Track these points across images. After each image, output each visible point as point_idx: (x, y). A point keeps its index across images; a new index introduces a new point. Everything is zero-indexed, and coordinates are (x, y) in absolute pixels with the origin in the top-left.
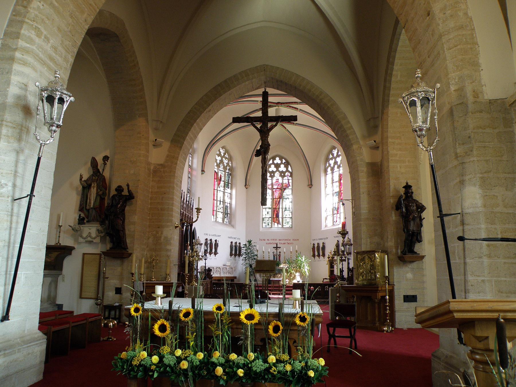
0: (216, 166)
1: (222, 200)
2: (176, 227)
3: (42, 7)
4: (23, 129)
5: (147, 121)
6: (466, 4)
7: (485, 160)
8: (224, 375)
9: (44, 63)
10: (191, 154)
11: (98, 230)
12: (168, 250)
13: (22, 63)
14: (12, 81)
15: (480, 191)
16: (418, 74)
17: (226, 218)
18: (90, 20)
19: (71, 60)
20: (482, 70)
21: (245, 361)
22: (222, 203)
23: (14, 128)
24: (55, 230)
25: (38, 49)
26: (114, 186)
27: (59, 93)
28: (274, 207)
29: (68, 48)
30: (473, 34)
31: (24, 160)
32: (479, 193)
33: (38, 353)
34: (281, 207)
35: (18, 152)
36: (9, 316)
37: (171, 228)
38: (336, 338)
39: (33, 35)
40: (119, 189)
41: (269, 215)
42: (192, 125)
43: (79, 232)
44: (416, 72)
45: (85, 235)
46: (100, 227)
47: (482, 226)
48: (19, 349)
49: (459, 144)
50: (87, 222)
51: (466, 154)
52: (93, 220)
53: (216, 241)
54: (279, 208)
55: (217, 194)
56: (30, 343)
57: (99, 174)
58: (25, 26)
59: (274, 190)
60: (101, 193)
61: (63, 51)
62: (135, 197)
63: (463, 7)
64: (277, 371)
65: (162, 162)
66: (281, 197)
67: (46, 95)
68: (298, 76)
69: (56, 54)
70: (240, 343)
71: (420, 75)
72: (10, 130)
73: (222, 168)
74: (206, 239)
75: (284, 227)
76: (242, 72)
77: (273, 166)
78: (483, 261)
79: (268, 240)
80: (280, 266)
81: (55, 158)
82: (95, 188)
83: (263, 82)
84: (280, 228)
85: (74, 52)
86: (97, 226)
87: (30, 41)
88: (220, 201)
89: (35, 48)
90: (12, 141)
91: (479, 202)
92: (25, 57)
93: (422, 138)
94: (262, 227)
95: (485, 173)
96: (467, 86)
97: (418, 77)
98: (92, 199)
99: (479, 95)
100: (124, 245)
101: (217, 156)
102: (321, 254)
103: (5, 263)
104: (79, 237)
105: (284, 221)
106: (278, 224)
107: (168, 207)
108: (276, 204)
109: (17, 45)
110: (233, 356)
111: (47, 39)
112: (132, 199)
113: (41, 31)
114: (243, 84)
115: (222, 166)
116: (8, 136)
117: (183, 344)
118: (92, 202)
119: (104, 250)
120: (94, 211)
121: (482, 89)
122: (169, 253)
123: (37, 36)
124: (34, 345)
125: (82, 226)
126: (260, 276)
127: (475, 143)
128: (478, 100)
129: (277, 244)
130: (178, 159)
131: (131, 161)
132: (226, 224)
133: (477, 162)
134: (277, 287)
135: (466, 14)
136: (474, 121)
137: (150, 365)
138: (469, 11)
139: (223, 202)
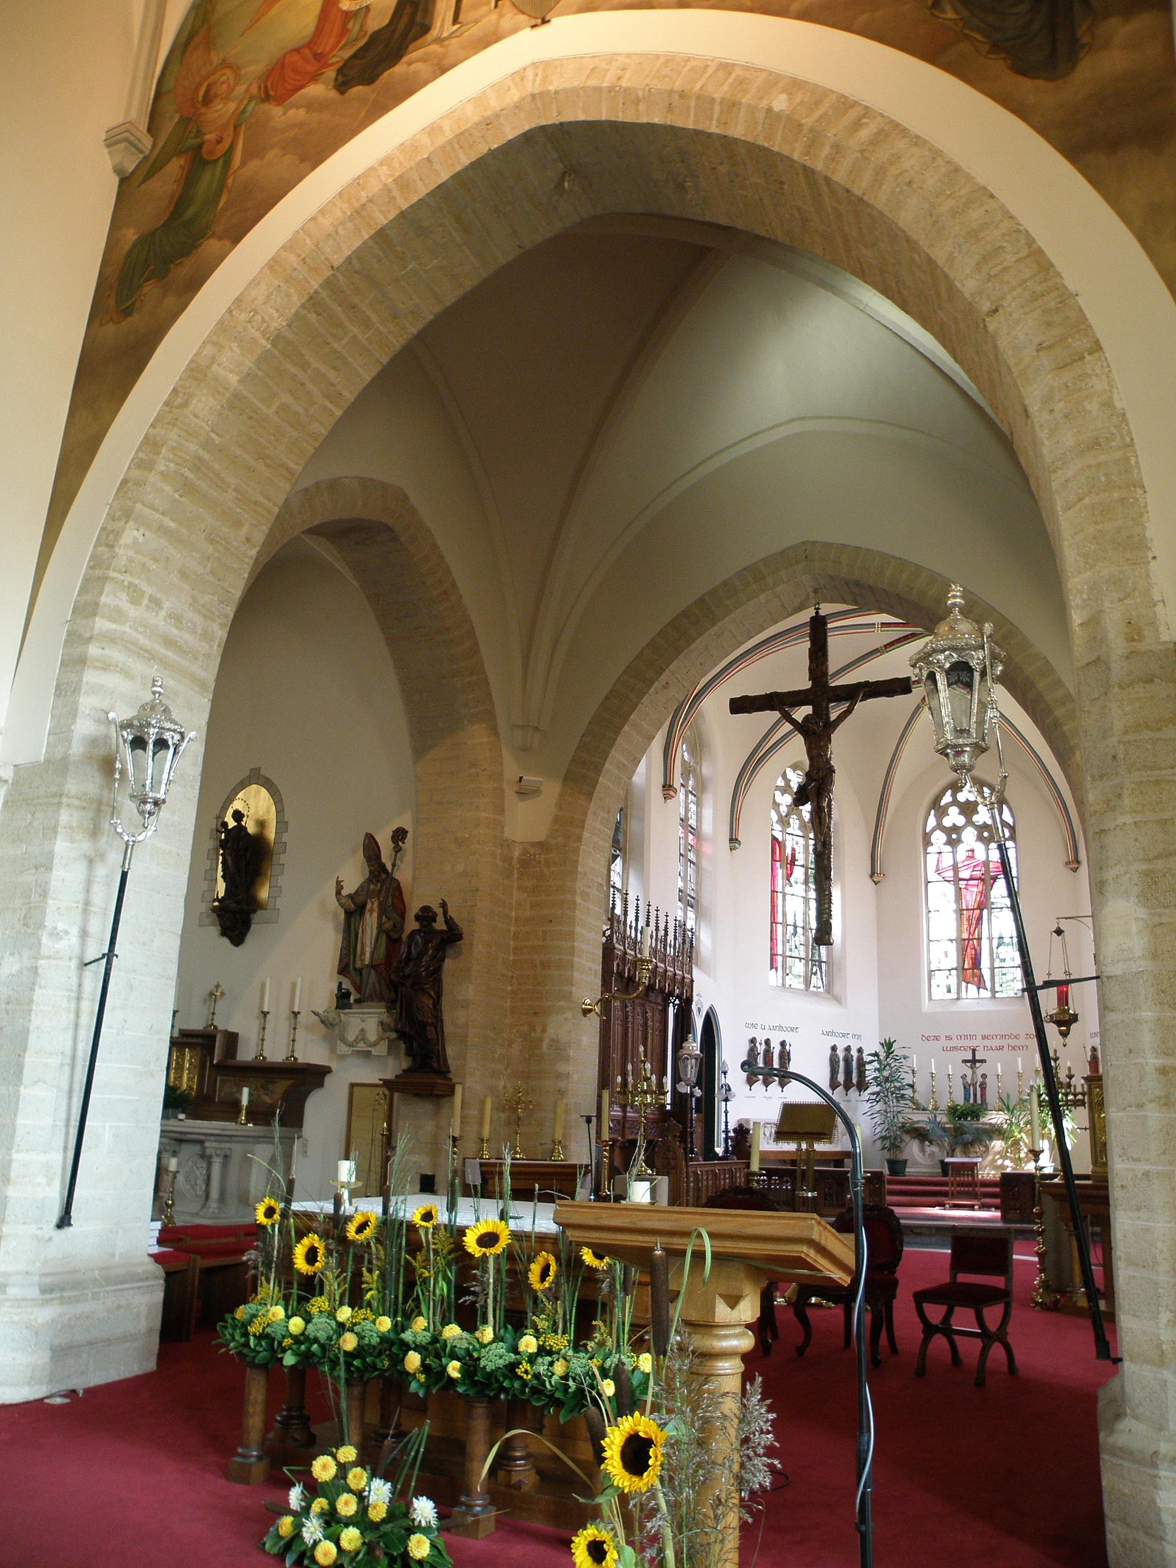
0: (777, 822)
1: (800, 923)
2: (586, 1012)
3: (141, 539)
4: (103, 808)
5: (494, 731)
6: (1108, 377)
7: (1158, 821)
8: (422, 1372)
9: (150, 656)
10: (692, 794)
11: (382, 1023)
12: (559, 1076)
13: (102, 665)
14: (81, 709)
15: (1142, 912)
16: (954, 597)
17: (815, 974)
18: (259, 537)
19: (220, 634)
20: (1154, 558)
21: (470, 1344)
22: (800, 931)
23: (84, 808)
24: (287, 1023)
25: (136, 630)
26: (413, 908)
27: (156, 730)
28: (965, 936)
29: (208, 610)
30: (1127, 459)
31: (107, 876)
32: (1137, 919)
33: (143, 1310)
34: (985, 935)
35: (91, 861)
36: (70, 1218)
37: (569, 1015)
38: (956, 1337)
39: (122, 601)
40: (426, 916)
41: (952, 961)
42: (618, 730)
43: (337, 1029)
44: (949, 592)
45: (351, 1038)
46: (385, 1015)
47: (1143, 1014)
48: (93, 1293)
49: (1093, 776)
50: (357, 1001)
51: (1108, 805)
52: (371, 998)
53: (783, 1044)
54: (979, 939)
55: (784, 906)
56: (122, 1283)
57: (384, 876)
58: (108, 587)
59: (961, 882)
60: (388, 925)
61: (198, 619)
62: (464, 935)
63: (1099, 385)
64: (531, 1373)
65: (541, 838)
66: (984, 904)
67: (130, 738)
68: (902, 563)
69: (179, 629)
70: (465, 1301)
71: (958, 600)
72: (76, 814)
73: (797, 826)
74: (753, 1041)
75: (997, 995)
76: (745, 569)
77: (953, 811)
78: (1145, 1116)
79: (949, 1038)
80: (982, 1120)
81: (188, 864)
82: (375, 915)
83: (809, 590)
84: (985, 1001)
85: (226, 616)
86: (380, 1013)
87: (118, 615)
88: (795, 927)
89: (127, 629)
90: (78, 836)
91: (1138, 944)
92: (107, 652)
93: (961, 773)
94: (930, 998)
95: (1157, 858)
96: (1108, 611)
97: (954, 605)
98: (368, 942)
99: (1146, 633)
100: (438, 1061)
101: (778, 793)
102: (854, 1081)
103: (64, 1103)
104: (339, 1042)
105: (997, 979)
106: (979, 989)
107: (558, 957)
108: (970, 925)
109: (92, 629)
110: (452, 1331)
111: (155, 603)
112: (459, 940)
113: (141, 589)
114: (751, 603)
115: (797, 822)
116: (71, 828)
117: (355, 1298)
118: (368, 950)
119: (389, 1076)
120: (372, 971)
121: (1155, 613)
122: (562, 1084)
123: (132, 603)
124: (132, 1288)
125: (345, 1014)
126: (923, 1151)
127: (1130, 772)
128: (1140, 647)
129: (974, 1051)
130: (583, 827)
131: (456, 840)
132: (815, 994)
133: (1133, 827)
134: (968, 1185)
135: (1108, 404)
136: (1128, 709)
137: (284, 1337)
138: (1116, 397)
139: (803, 928)
